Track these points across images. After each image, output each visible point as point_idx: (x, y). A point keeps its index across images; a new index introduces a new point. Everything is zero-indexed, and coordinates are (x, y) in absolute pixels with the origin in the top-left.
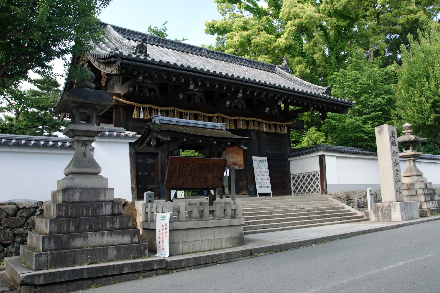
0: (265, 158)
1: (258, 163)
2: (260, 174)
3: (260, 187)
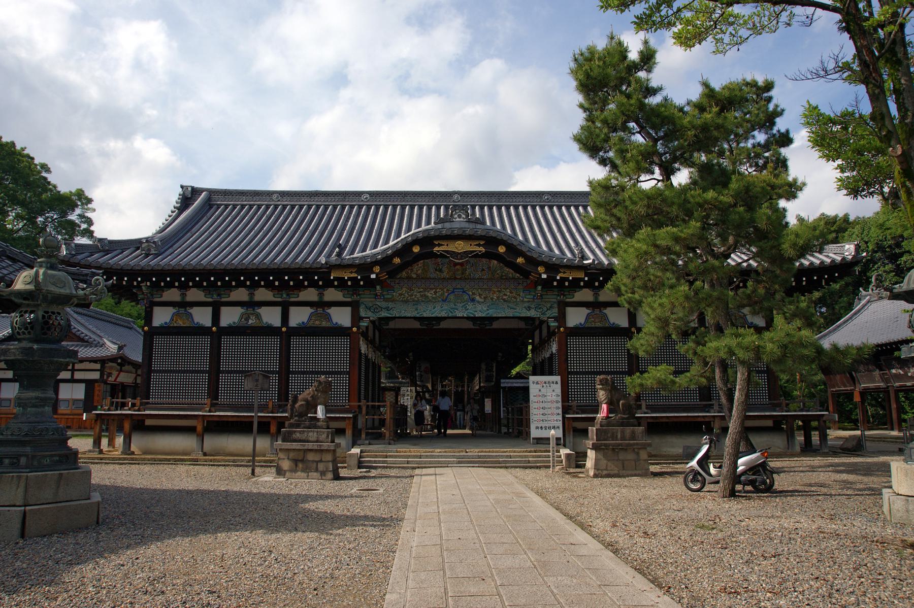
0: (558, 378)
1: (539, 386)
2: (542, 405)
3: (537, 428)
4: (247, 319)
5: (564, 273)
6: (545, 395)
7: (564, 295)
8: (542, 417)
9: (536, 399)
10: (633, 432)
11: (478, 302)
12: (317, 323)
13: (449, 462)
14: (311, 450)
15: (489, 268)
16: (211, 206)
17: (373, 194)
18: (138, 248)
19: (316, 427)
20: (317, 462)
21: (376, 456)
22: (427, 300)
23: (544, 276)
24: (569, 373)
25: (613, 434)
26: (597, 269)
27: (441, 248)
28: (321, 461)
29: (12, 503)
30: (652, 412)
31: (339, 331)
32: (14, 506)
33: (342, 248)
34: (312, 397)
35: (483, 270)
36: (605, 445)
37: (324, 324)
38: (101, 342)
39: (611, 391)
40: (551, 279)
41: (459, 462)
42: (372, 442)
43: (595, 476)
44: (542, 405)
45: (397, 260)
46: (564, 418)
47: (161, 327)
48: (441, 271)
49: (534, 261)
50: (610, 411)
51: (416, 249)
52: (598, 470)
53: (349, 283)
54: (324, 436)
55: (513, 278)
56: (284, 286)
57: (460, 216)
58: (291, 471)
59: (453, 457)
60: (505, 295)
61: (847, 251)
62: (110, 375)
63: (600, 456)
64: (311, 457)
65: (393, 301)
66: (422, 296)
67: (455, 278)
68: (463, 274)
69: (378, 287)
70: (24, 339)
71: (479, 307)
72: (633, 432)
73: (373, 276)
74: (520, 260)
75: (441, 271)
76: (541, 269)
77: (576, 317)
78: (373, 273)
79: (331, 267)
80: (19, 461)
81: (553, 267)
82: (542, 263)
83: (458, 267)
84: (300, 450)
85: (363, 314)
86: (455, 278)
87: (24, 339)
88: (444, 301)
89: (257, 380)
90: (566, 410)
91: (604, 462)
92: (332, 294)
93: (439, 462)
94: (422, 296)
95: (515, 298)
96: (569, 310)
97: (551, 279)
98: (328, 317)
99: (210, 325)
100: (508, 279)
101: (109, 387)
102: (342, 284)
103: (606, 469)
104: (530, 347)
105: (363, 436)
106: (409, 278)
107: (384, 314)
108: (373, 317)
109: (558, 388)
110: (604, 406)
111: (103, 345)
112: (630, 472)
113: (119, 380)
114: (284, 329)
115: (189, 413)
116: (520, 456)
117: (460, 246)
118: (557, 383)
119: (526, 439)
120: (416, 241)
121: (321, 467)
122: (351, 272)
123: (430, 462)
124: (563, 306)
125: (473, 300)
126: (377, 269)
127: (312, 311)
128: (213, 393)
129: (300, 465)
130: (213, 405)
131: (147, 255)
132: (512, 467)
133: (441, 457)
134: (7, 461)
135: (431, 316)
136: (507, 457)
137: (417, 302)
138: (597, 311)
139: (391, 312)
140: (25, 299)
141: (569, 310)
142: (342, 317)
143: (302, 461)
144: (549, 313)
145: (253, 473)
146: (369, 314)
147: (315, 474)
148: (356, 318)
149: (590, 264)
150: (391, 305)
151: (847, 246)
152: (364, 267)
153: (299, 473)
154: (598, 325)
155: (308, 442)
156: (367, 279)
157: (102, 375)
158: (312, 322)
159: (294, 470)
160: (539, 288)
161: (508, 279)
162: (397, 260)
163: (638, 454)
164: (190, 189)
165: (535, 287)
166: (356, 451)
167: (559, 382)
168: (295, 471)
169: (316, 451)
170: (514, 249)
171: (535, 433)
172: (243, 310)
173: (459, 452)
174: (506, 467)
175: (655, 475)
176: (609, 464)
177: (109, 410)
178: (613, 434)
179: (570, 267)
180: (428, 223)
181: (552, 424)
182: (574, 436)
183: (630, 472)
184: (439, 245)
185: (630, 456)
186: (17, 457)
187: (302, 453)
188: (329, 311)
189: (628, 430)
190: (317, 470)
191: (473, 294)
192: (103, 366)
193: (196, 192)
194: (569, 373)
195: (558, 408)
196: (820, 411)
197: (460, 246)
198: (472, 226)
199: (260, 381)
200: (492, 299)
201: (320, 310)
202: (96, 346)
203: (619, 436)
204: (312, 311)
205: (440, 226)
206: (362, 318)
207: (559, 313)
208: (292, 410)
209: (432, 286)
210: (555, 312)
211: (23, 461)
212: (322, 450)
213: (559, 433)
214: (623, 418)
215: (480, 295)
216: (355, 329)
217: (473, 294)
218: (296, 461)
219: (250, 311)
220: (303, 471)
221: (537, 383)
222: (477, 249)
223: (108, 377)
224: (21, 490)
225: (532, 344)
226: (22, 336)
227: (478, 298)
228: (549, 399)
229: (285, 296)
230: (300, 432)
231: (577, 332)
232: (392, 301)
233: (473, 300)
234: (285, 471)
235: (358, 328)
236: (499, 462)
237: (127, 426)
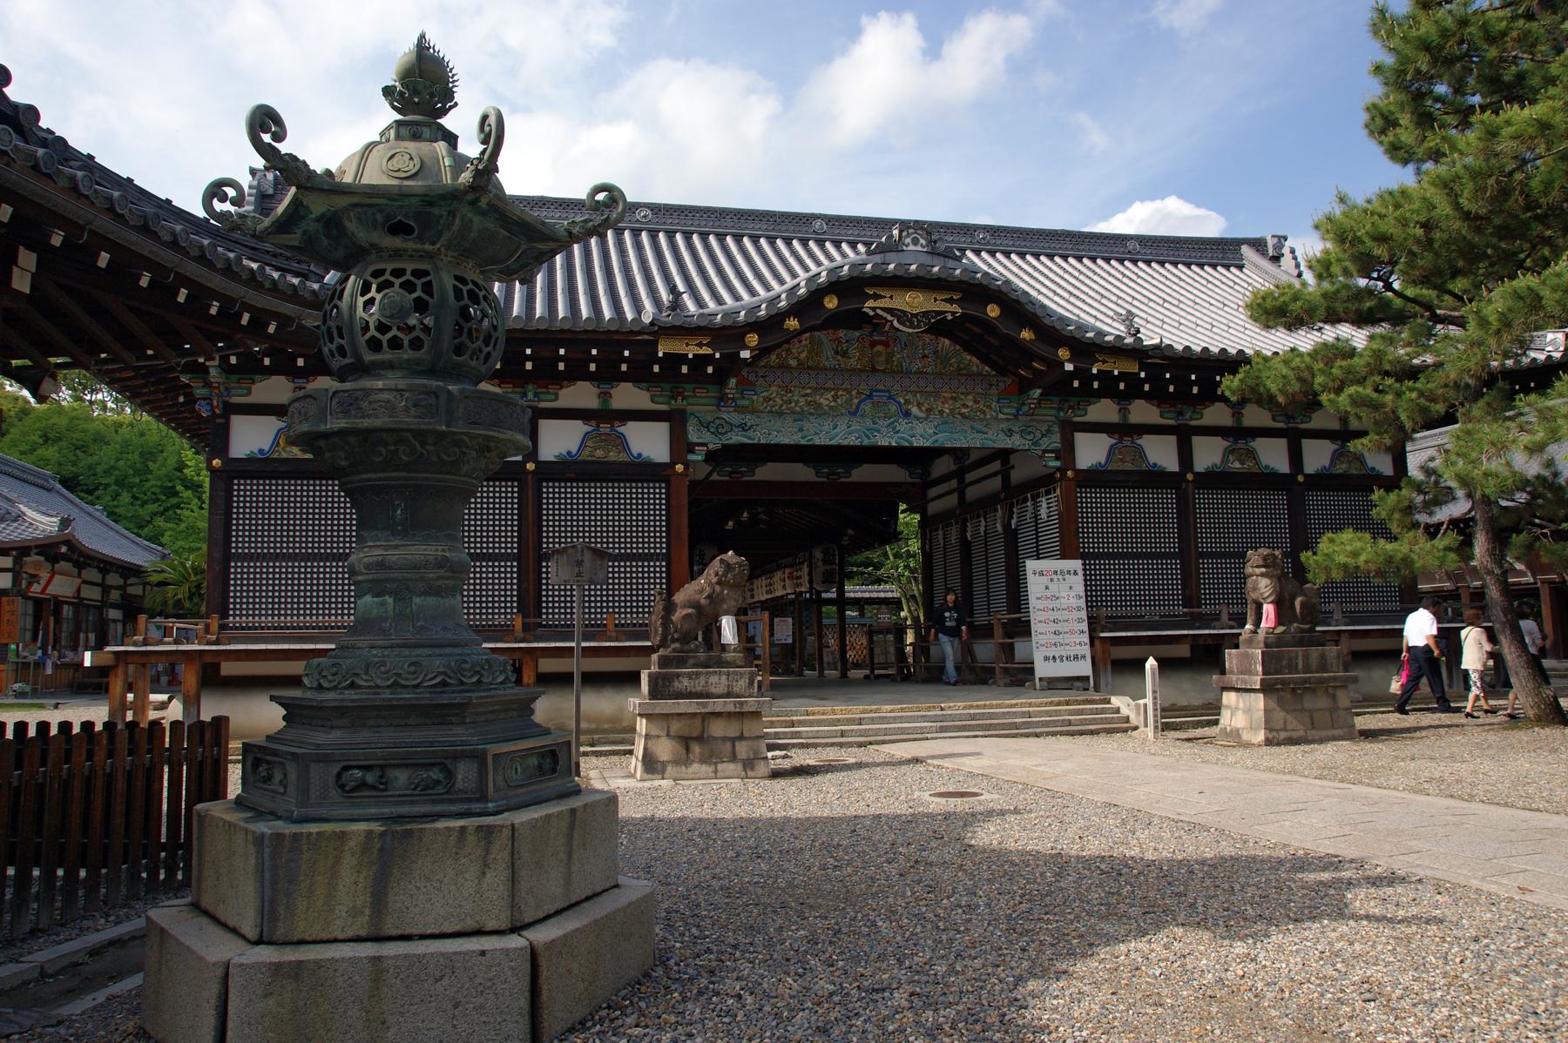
1: (1045, 580)
2: (1052, 615)
3: (1046, 659)
5: (1104, 362)
6: (1056, 593)
8: (1053, 639)
9: (1040, 604)
10: (1323, 657)
11: (917, 418)
12: (599, 453)
13: (922, 730)
19: (721, 663)
20: (733, 740)
22: (818, 412)
26: (1163, 358)
28: (741, 737)
29: (470, 924)
31: (643, 471)
32: (479, 932)
34: (709, 597)
35: (925, 356)
36: (1284, 682)
37: (613, 456)
38: (14, 512)
39: (1279, 579)
41: (943, 729)
43: (1269, 742)
44: (1052, 615)
45: (792, 323)
47: (250, 460)
48: (845, 354)
50: (1280, 620)
51: (831, 303)
52: (1271, 730)
54: (742, 683)
55: (980, 374)
58: (677, 762)
59: (924, 719)
60: (964, 405)
61: (1551, 343)
62: (34, 578)
63: (1273, 704)
64: (718, 729)
66: (809, 403)
67: (874, 370)
68: (887, 361)
70: (390, 366)
71: (919, 428)
72: (1323, 657)
74: (1026, 335)
75: (845, 354)
76: (1063, 353)
77: (1091, 451)
78: (746, 347)
80: (449, 774)
83: (879, 348)
84: (695, 714)
85: (693, 435)
86: (874, 370)
87: (390, 366)
88: (854, 414)
89: (580, 563)
91: (1280, 715)
93: (903, 731)
94: (809, 403)
95: (984, 413)
96: (1081, 438)
100: (970, 375)
101: (30, 603)
106: (784, 366)
107: (737, 438)
108: (714, 443)
110: (1269, 610)
111: (20, 517)
112: (1324, 733)
113: (51, 590)
115: (293, 647)
116: (1048, 713)
117: (913, 302)
118: (1075, 573)
122: (700, 345)
123: (886, 732)
124: (1070, 429)
126: (753, 339)
127: (589, 429)
129: (696, 749)
132: (1048, 734)
133: (895, 719)
134: (401, 777)
135: (829, 443)
136: (1023, 714)
137: (800, 416)
140: (398, 229)
141: (1081, 438)
142: (649, 442)
143: (700, 739)
144: (1045, 443)
146: (707, 437)
147: (731, 766)
148: (680, 445)
150: (749, 419)
151: (1550, 336)
153: (695, 767)
154: (1129, 466)
155: (708, 696)
157: (16, 580)
158: (587, 452)
159: (683, 760)
161: (970, 375)
163: (1334, 697)
167: (1081, 572)
168: (687, 762)
169: (729, 715)
173: (929, 709)
174: (1037, 735)
175: (1369, 735)
176: (1289, 718)
177: (161, 642)
178: (1290, 660)
182: (1113, 671)
183: (1324, 733)
184: (876, 297)
185: (1322, 702)
186: (445, 763)
187: (697, 722)
188: (621, 429)
189: (1315, 652)
190: (734, 758)
195: (1080, 620)
196: (1232, 627)
199: (587, 564)
200: (941, 412)
202: (15, 520)
203: (1300, 665)
204: (589, 429)
206: (691, 448)
209: (830, 384)
210: (1054, 441)
211: (465, 773)
212: (742, 714)
214: (1303, 631)
215: (919, 405)
216: (679, 468)
218: (686, 741)
220: (702, 761)
221: (1041, 574)
222: (947, 307)
223: (30, 584)
224: (496, 878)
226: (387, 355)
227: (915, 410)
228: (1064, 602)
229: (530, 395)
230: (689, 676)
231: (1095, 478)
233: (907, 414)
234: (664, 764)
235: (686, 465)
237: (190, 677)
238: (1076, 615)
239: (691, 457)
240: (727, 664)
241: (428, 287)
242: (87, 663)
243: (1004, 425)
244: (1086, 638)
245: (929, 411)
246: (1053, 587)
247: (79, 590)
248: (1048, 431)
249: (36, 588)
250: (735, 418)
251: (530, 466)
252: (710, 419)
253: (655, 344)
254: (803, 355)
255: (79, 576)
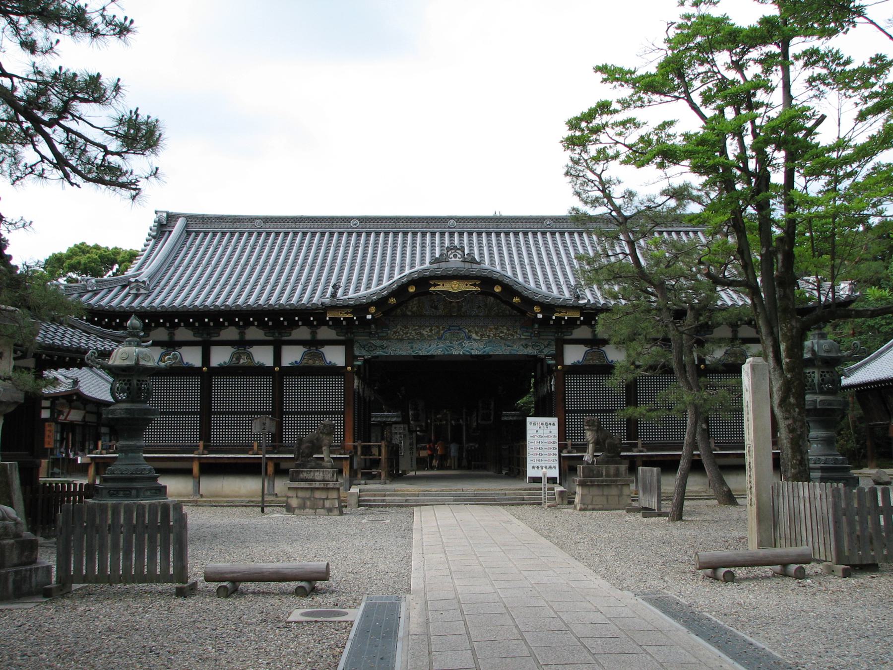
0: (555, 420)
1: (536, 427)
3: (533, 467)
4: (238, 359)
5: (560, 312)
6: (542, 437)
7: (562, 333)
11: (475, 340)
14: (318, 489)
15: (486, 305)
16: (189, 234)
17: (364, 220)
18: (124, 287)
20: (324, 500)
21: (375, 495)
22: (422, 339)
23: (540, 316)
24: (567, 412)
25: (598, 471)
27: (437, 288)
28: (327, 498)
30: (648, 451)
31: (333, 371)
33: (336, 287)
35: (479, 307)
37: (318, 363)
40: (547, 319)
41: (455, 500)
42: (368, 481)
43: (580, 510)
45: (393, 301)
46: (560, 456)
48: (436, 308)
49: (529, 302)
51: (412, 289)
53: (344, 323)
56: (278, 325)
57: (455, 256)
60: (502, 332)
65: (389, 339)
66: (417, 334)
69: (373, 326)
71: (475, 345)
73: (369, 317)
74: (516, 300)
75: (436, 308)
78: (369, 313)
79: (326, 308)
81: (549, 307)
82: (538, 303)
85: (357, 353)
86: (451, 316)
88: (440, 339)
90: (561, 448)
92: (325, 333)
93: (437, 500)
94: (417, 334)
95: (512, 335)
97: (547, 319)
98: (321, 356)
99: (200, 365)
101: (59, 426)
102: (336, 322)
103: (592, 504)
104: (533, 380)
105: (359, 476)
109: (555, 430)
110: (591, 446)
114: (277, 369)
119: (523, 479)
120: (412, 282)
121: (328, 504)
122: (347, 313)
124: (560, 344)
125: (469, 338)
128: (205, 434)
130: (205, 447)
131: (137, 296)
137: (412, 341)
138: (595, 349)
139: (386, 350)
142: (335, 356)
144: (546, 351)
145: (263, 511)
146: (364, 353)
148: (350, 357)
149: (585, 304)
150: (385, 343)
152: (359, 308)
153: (307, 510)
154: (597, 362)
155: (315, 481)
156: (362, 319)
157: (52, 414)
159: (303, 507)
160: (536, 326)
162: (393, 301)
164: (165, 215)
165: (533, 325)
166: (355, 490)
167: (556, 424)
170: (510, 289)
171: (531, 472)
172: (233, 350)
179: (565, 307)
180: (422, 262)
181: (548, 464)
184: (435, 285)
190: (323, 507)
191: (470, 331)
192: (53, 403)
193: (172, 218)
194: (567, 412)
197: (455, 287)
198: (468, 265)
199: (267, 424)
200: (489, 336)
201: (313, 349)
204: (305, 350)
205: (435, 266)
206: (355, 358)
207: (556, 351)
208: (299, 450)
210: (552, 350)
212: (328, 489)
213: (555, 473)
215: (476, 333)
216: (349, 368)
217: (470, 331)
219: (241, 350)
221: (535, 424)
223: (59, 416)
225: (535, 377)
227: (474, 336)
231: (575, 369)
232: (387, 340)
233: (469, 338)
234: (294, 509)
236: (495, 500)
238: (552, 446)
239: (356, 363)
240: (324, 467)
241: (130, 384)
242: (79, 462)
243: (523, 342)
244: (557, 458)
245: (482, 336)
246: (541, 432)
247: (84, 417)
248: (548, 345)
249: (62, 417)
250: (378, 343)
251: (277, 369)
252: (365, 343)
253: (325, 315)
254: (414, 309)
255: (85, 409)
